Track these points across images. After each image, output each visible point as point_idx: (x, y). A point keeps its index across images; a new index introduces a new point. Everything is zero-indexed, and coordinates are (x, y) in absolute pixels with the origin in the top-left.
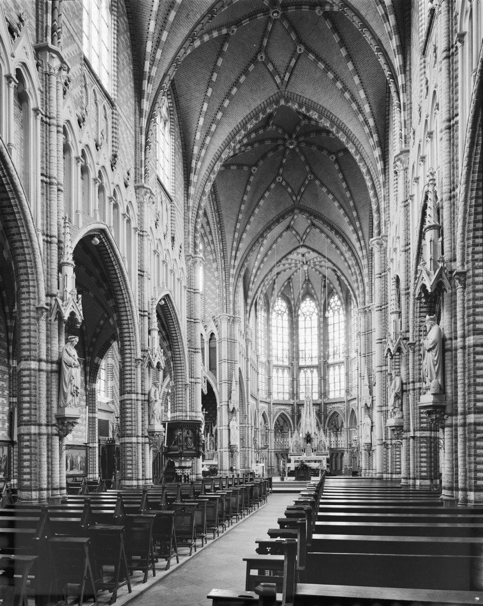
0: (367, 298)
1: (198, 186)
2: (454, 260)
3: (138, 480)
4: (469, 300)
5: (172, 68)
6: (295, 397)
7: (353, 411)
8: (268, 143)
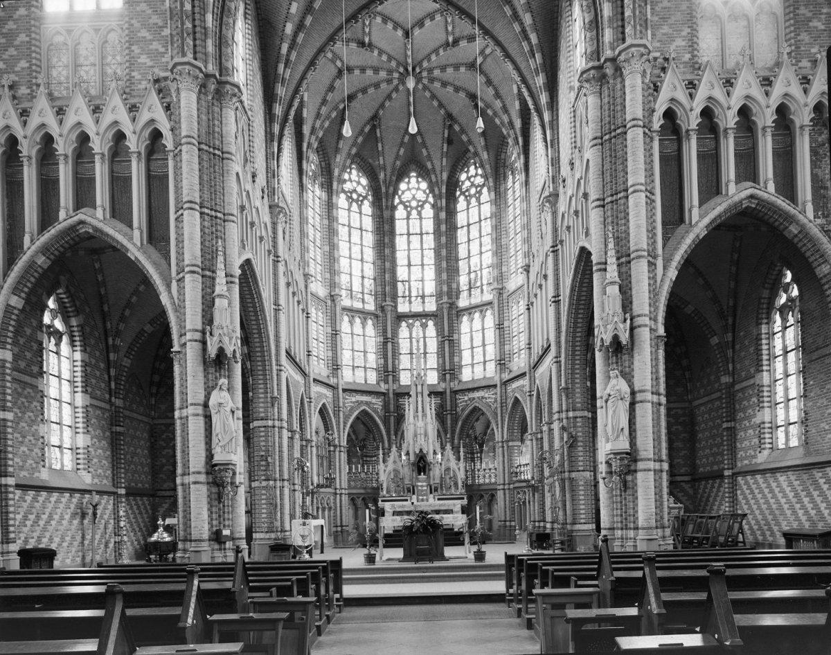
6: (390, 378)
7: (517, 401)
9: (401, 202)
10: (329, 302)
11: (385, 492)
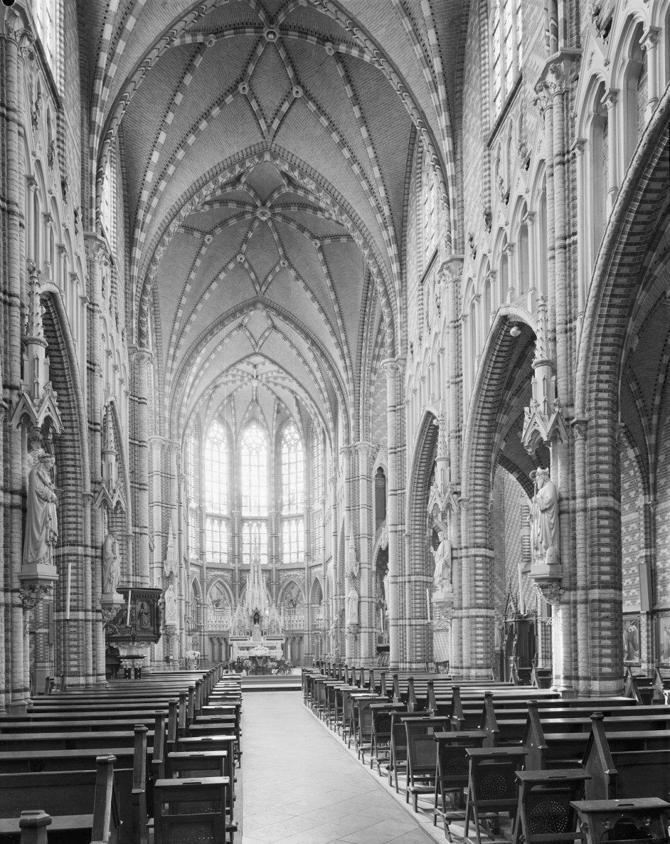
0: (352, 434)
1: (146, 248)
3: (87, 675)
5: (139, 74)
7: (317, 580)
8: (232, 206)
10: (199, 512)
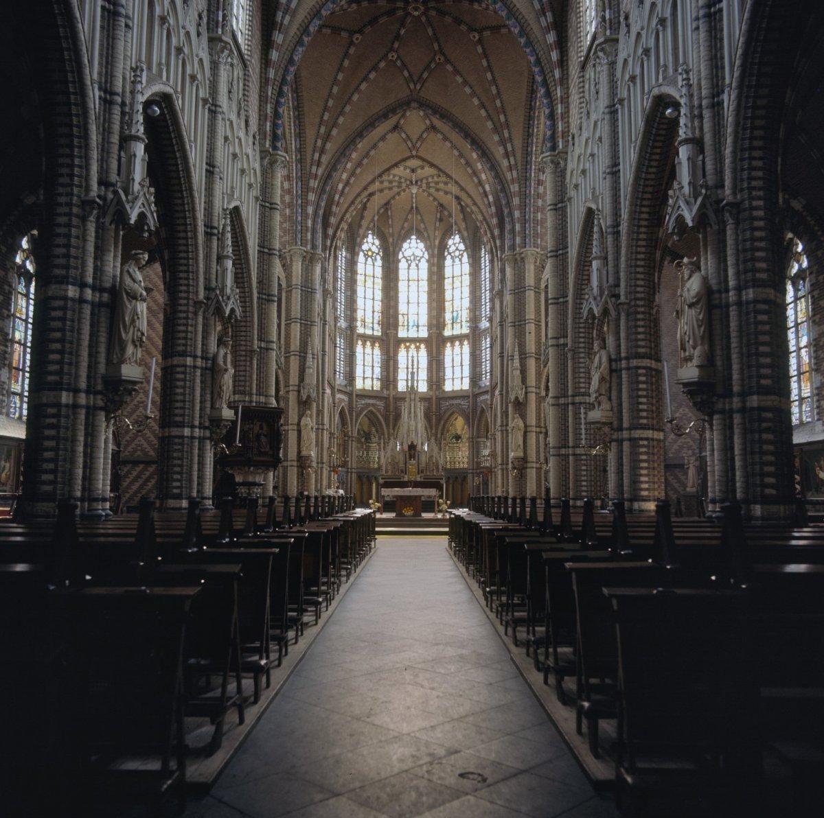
0: (518, 240)
2: (721, 186)
4: (745, 241)
9: (404, 257)
11: (384, 472)
